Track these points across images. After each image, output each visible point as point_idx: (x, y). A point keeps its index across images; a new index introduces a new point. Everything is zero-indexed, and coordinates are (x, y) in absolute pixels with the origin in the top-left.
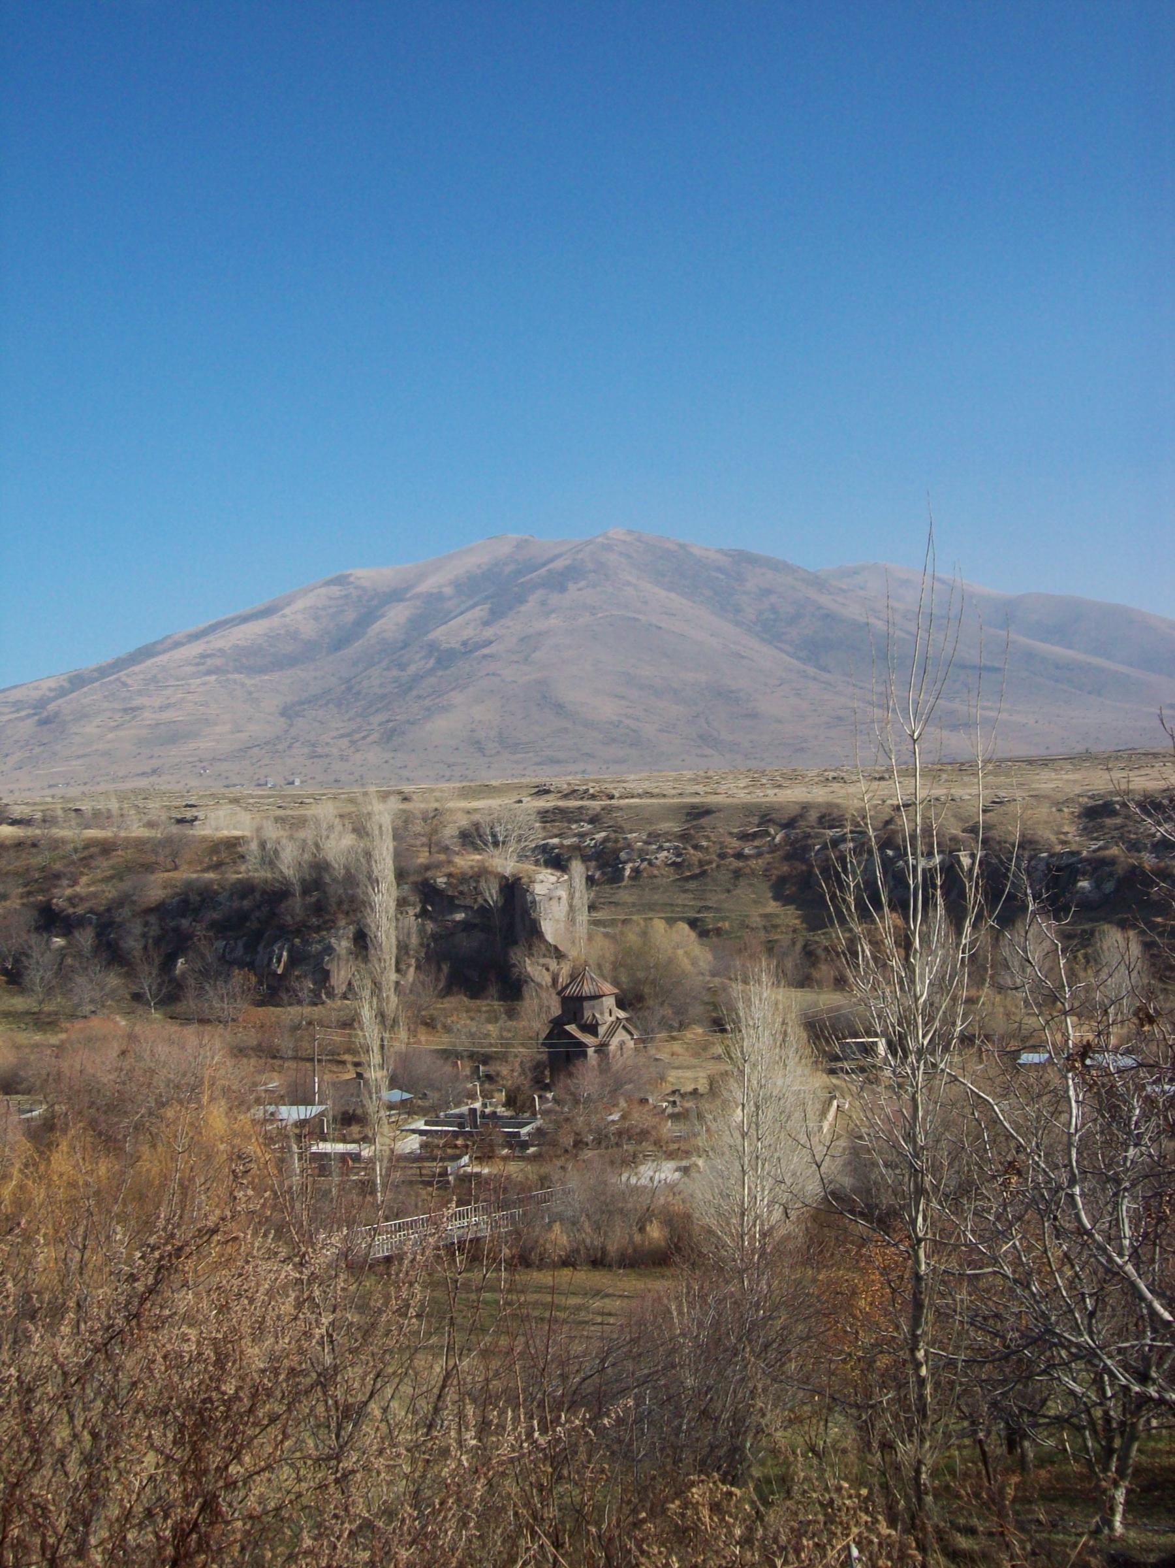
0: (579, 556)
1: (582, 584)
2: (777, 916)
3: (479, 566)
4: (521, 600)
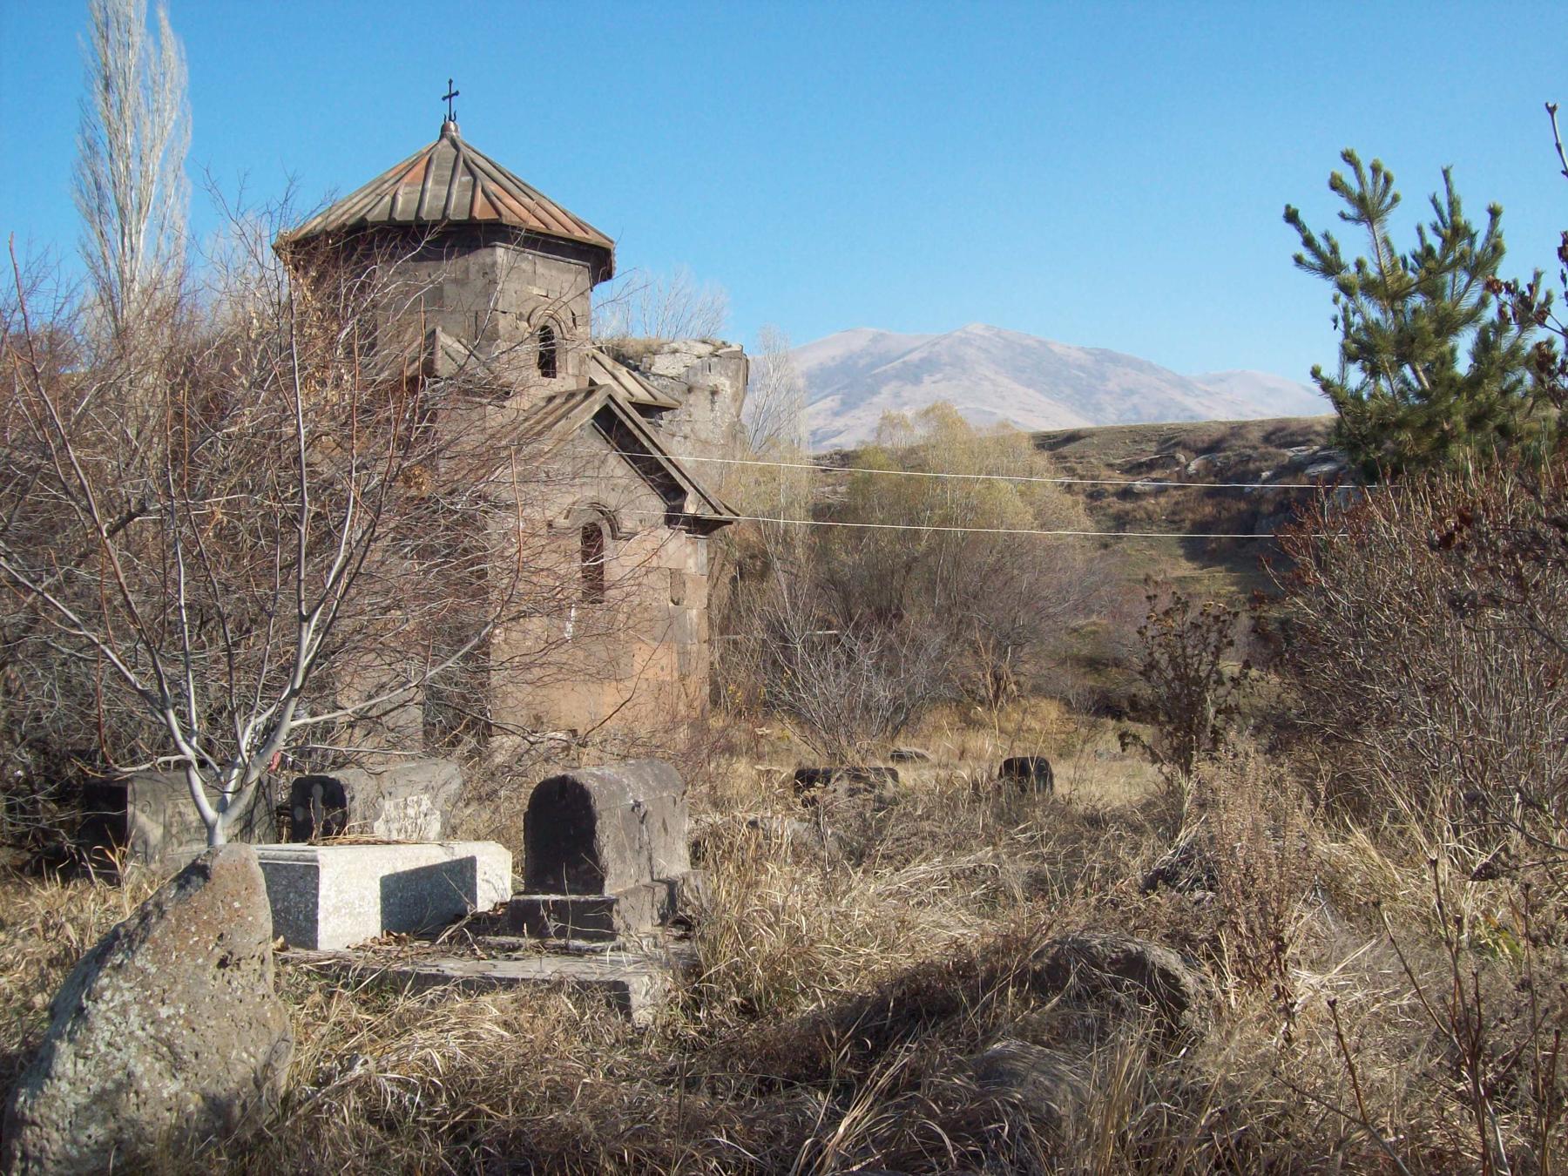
0: (937, 348)
1: (939, 376)
2: (1197, 580)
4: (874, 392)
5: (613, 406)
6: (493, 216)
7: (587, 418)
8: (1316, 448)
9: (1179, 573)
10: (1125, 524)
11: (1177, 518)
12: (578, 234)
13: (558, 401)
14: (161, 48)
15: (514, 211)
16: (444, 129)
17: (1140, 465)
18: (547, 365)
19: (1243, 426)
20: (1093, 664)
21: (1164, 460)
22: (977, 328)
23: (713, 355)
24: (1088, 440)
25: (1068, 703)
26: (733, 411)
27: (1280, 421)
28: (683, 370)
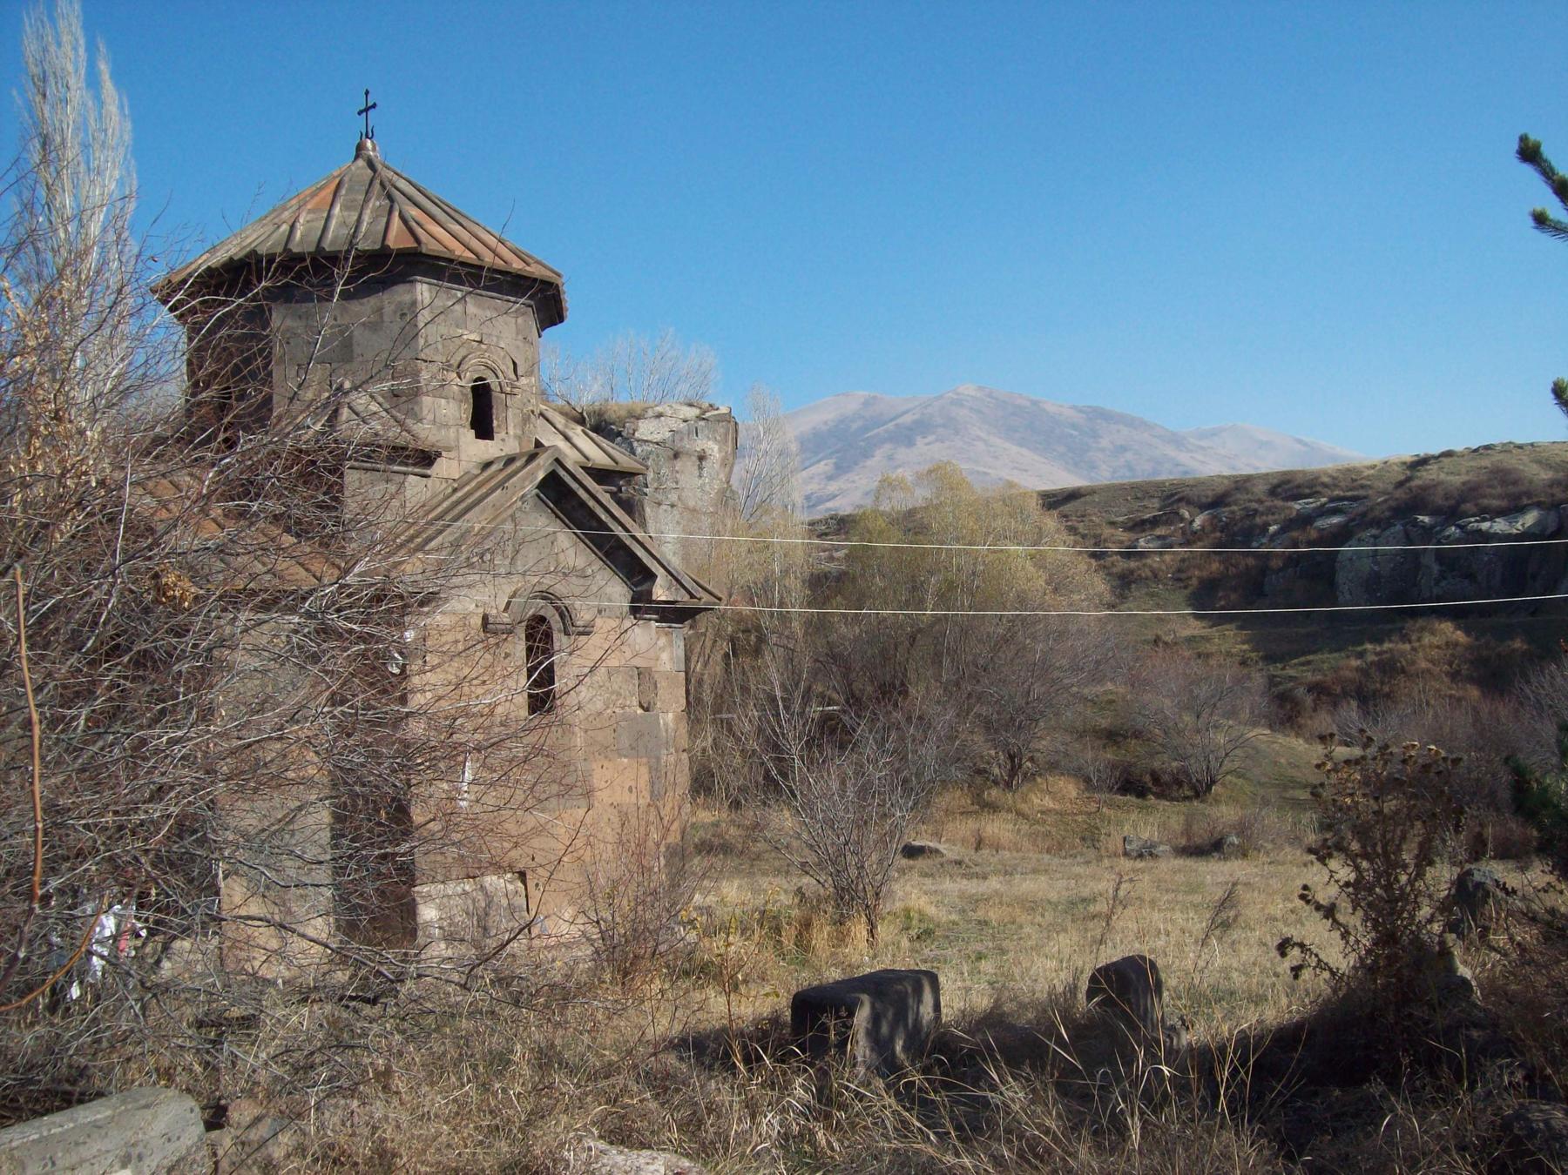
1: (931, 438)
2: (1207, 639)
3: (826, 423)
4: (867, 455)
5: (562, 473)
6: (412, 244)
7: (530, 488)
8: (1324, 500)
9: (1187, 633)
10: (1130, 583)
11: (1183, 576)
12: (517, 265)
13: (494, 468)
14: (100, 103)
15: (439, 238)
16: (360, 148)
17: (1143, 522)
18: (482, 426)
19: (1249, 479)
20: (1112, 737)
21: (1170, 517)
22: (968, 389)
23: (699, 418)
24: (1088, 498)
25: (1088, 780)
26: (722, 476)
27: (1285, 473)
28: (668, 434)
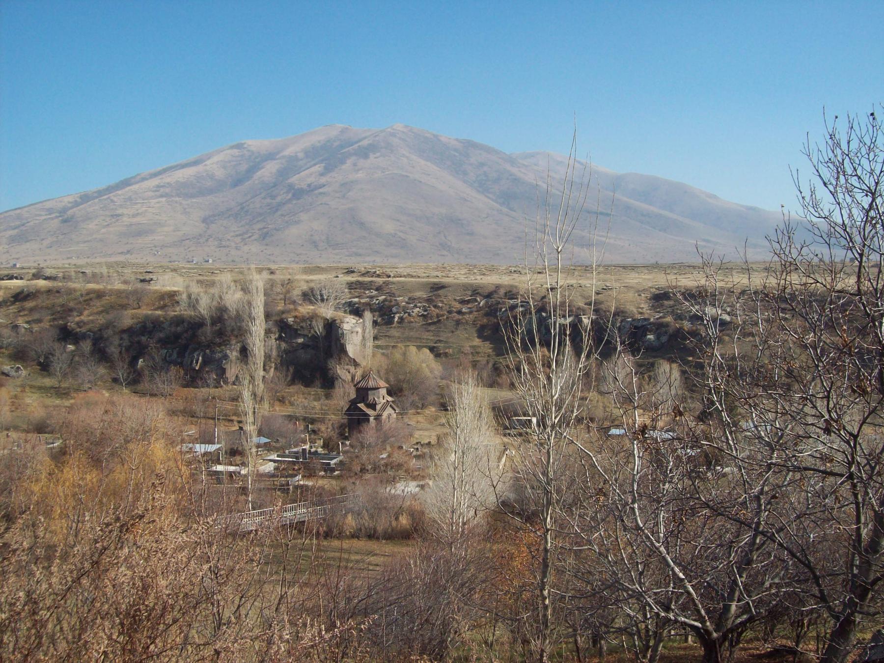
1: (378, 154)
3: (319, 142)
4: (342, 162)
